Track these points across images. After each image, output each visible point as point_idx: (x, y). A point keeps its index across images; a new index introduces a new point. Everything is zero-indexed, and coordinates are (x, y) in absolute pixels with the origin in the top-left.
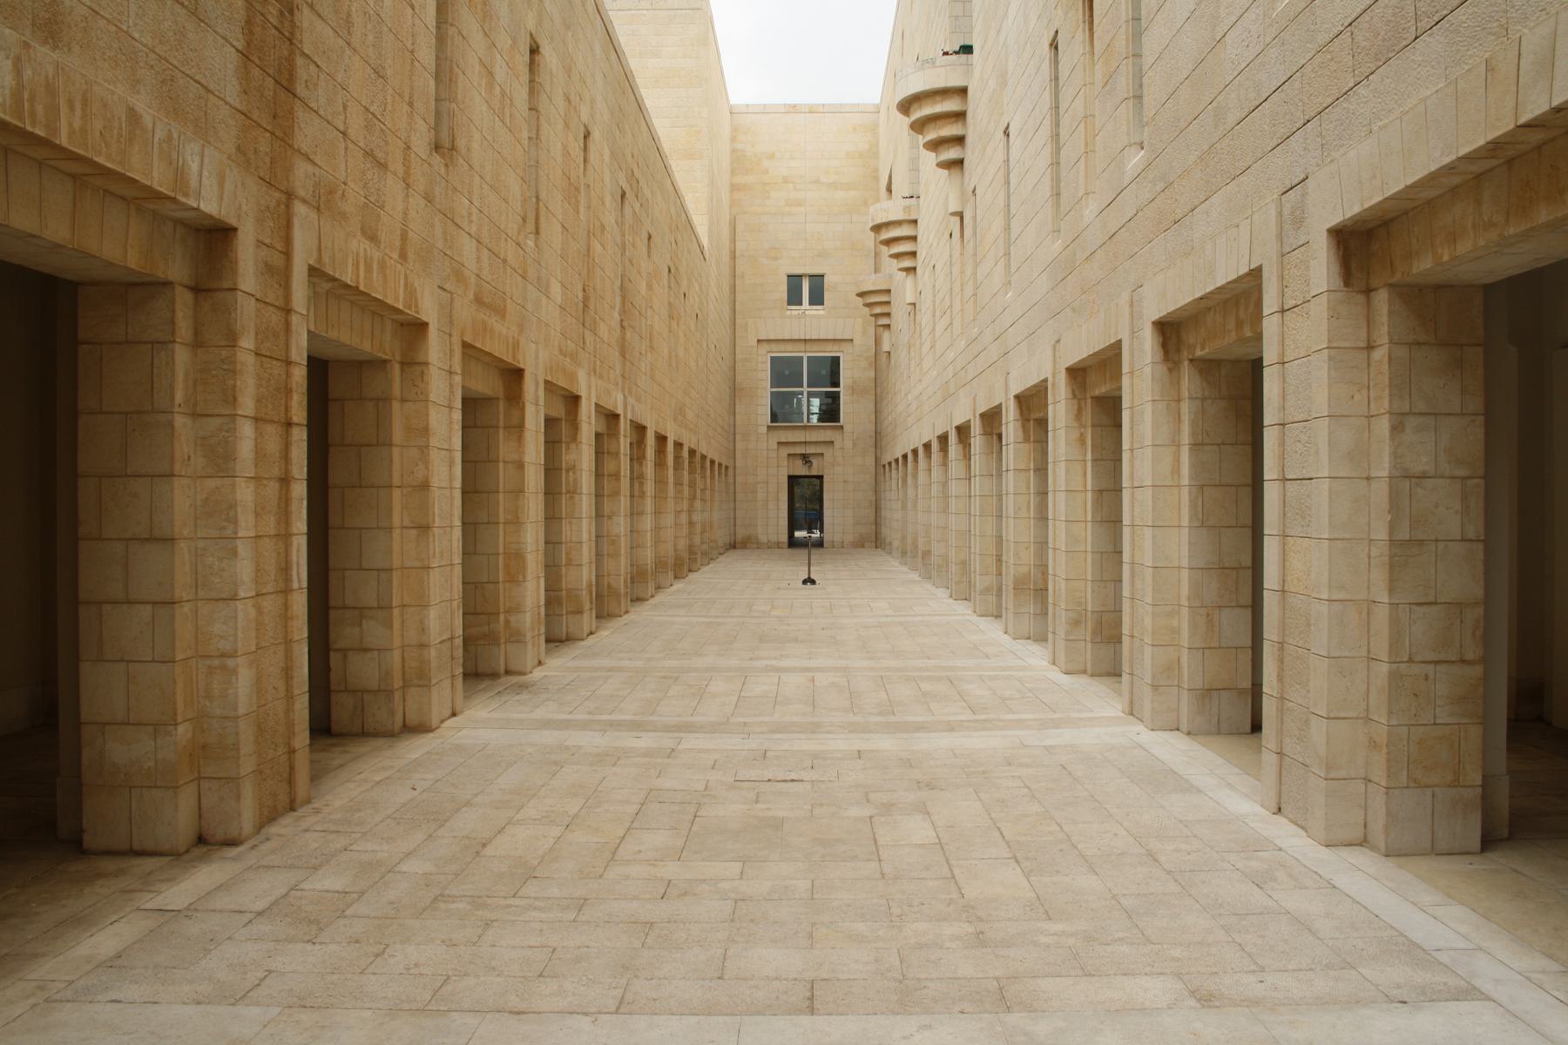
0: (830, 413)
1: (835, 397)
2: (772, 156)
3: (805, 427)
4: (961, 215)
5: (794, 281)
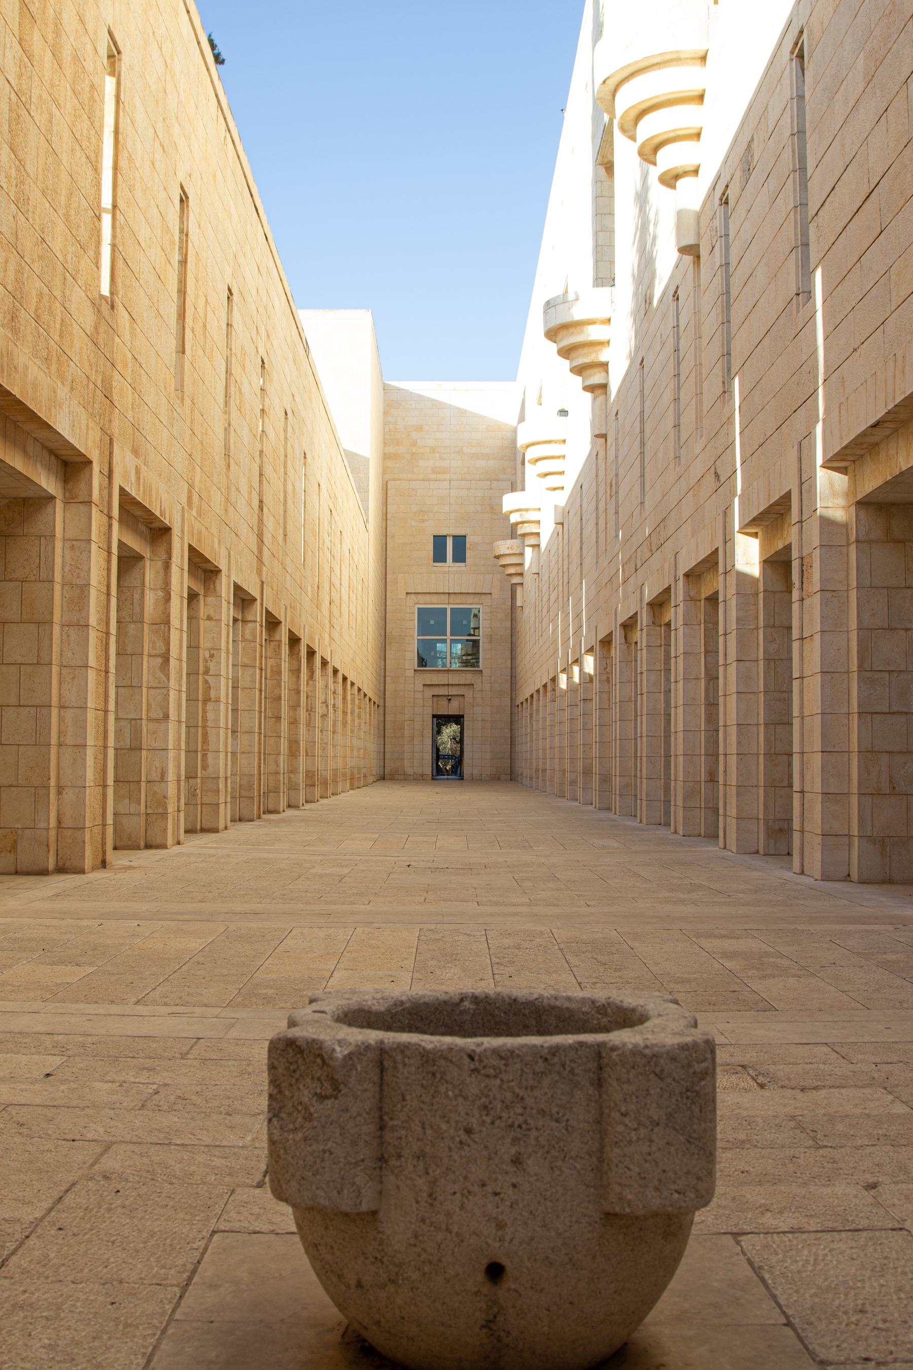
0: (471, 657)
1: (476, 643)
2: (419, 429)
3: (448, 671)
4: (562, 524)
5: (439, 542)
